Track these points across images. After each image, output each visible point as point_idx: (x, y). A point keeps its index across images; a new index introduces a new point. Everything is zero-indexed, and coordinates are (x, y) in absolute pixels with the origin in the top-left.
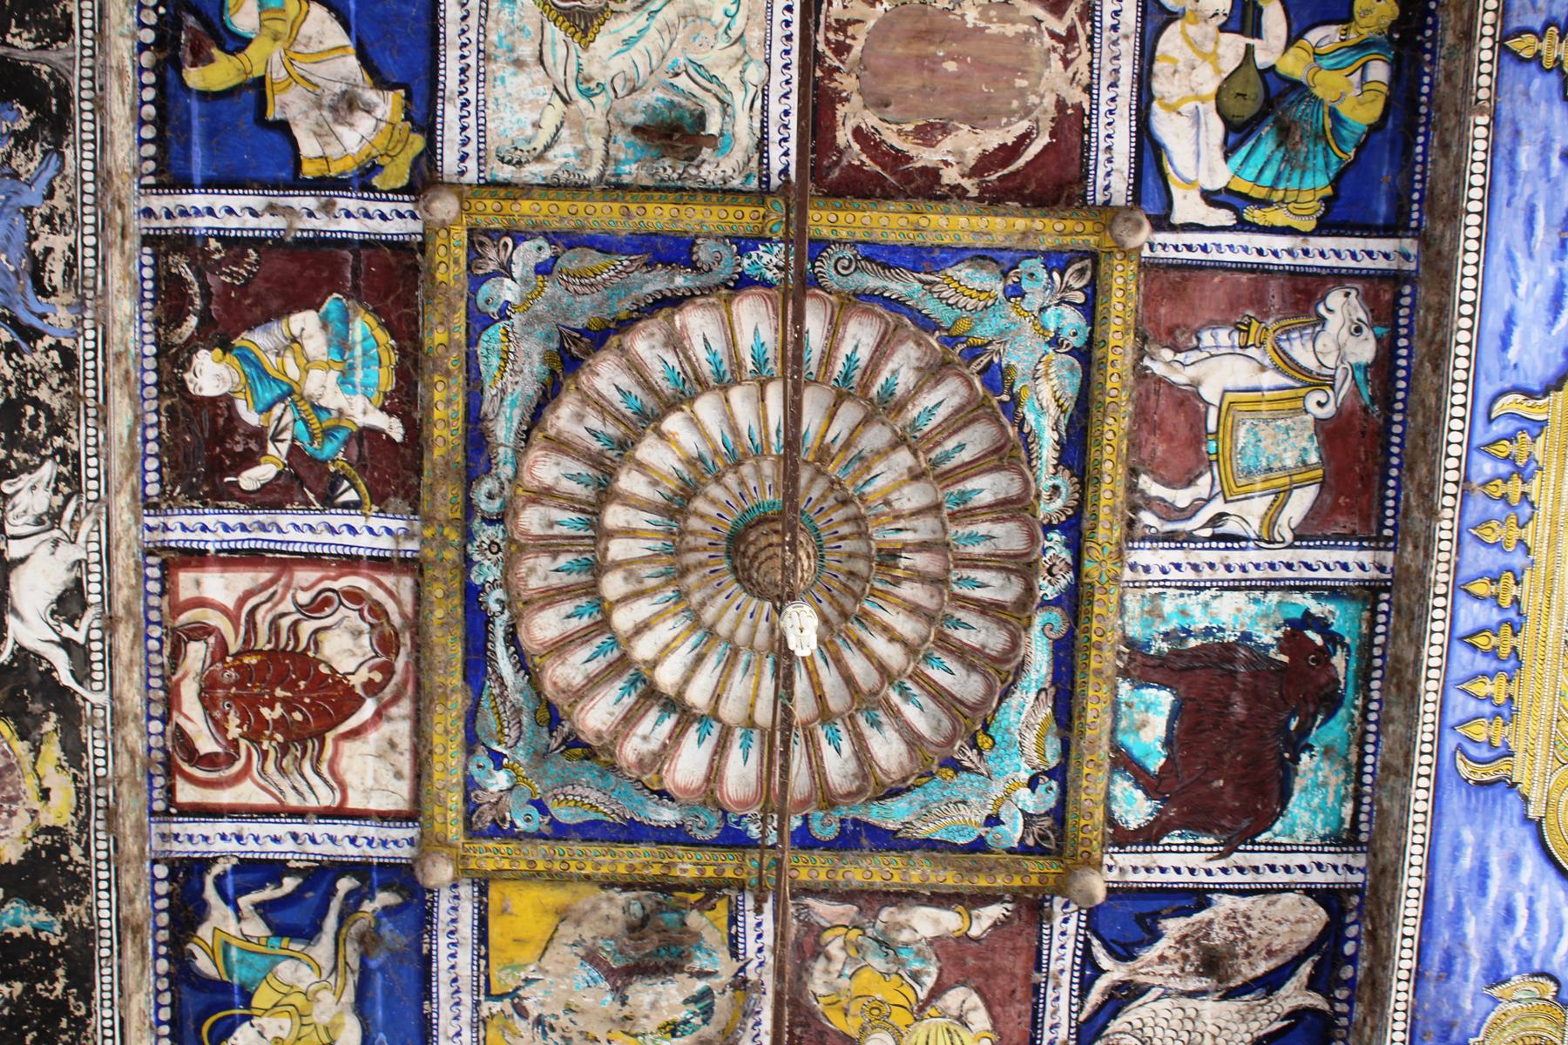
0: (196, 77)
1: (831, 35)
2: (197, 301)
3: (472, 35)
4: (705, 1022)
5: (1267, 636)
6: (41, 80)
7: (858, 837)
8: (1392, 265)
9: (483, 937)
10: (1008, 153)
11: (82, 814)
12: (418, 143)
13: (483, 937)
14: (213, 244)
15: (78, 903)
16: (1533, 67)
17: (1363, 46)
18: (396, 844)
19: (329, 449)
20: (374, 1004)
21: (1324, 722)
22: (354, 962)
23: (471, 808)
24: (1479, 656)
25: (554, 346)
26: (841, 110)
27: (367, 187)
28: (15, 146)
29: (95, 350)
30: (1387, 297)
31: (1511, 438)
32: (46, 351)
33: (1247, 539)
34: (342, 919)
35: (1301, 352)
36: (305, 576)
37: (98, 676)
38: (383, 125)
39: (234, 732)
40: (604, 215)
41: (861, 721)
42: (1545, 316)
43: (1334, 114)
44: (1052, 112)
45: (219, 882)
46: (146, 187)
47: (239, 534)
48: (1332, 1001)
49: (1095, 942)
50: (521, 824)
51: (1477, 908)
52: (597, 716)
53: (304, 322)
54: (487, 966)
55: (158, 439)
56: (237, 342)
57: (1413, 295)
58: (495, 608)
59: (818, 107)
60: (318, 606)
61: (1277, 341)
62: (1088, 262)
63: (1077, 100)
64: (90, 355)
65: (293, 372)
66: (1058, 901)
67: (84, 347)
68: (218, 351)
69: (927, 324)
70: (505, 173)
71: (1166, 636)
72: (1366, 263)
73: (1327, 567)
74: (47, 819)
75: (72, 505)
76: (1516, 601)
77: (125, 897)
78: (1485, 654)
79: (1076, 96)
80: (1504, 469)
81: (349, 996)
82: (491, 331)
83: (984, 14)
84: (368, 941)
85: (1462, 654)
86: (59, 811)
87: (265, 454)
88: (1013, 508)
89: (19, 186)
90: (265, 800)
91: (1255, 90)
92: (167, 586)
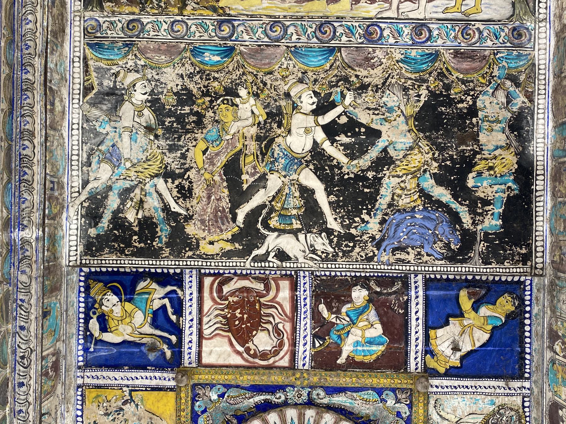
0: (463, 294)
2: (385, 291)
3: (479, 390)
9: (154, 389)
11: (204, 256)
12: (442, 370)
13: (154, 389)
14: (406, 298)
15: (170, 253)
18: (189, 358)
19: (334, 336)
20: (127, 348)
22: (144, 341)
23: (203, 386)
25: (372, 418)
27: (427, 352)
29: (373, 269)
32: (373, 251)
36: (288, 326)
37: (256, 264)
39: (231, 299)
45: (174, 292)
47: (303, 303)
53: (377, 330)
54: (142, 390)
55: (336, 275)
56: (371, 305)
58: (278, 396)
60: (278, 332)
64: (371, 267)
65: (361, 324)
70: (432, 402)
74: (202, 243)
75: (318, 258)
82: (377, 395)
84: (153, 348)
86: (205, 248)
87: (332, 314)
89: (431, 244)
90: (206, 309)
92: (284, 277)
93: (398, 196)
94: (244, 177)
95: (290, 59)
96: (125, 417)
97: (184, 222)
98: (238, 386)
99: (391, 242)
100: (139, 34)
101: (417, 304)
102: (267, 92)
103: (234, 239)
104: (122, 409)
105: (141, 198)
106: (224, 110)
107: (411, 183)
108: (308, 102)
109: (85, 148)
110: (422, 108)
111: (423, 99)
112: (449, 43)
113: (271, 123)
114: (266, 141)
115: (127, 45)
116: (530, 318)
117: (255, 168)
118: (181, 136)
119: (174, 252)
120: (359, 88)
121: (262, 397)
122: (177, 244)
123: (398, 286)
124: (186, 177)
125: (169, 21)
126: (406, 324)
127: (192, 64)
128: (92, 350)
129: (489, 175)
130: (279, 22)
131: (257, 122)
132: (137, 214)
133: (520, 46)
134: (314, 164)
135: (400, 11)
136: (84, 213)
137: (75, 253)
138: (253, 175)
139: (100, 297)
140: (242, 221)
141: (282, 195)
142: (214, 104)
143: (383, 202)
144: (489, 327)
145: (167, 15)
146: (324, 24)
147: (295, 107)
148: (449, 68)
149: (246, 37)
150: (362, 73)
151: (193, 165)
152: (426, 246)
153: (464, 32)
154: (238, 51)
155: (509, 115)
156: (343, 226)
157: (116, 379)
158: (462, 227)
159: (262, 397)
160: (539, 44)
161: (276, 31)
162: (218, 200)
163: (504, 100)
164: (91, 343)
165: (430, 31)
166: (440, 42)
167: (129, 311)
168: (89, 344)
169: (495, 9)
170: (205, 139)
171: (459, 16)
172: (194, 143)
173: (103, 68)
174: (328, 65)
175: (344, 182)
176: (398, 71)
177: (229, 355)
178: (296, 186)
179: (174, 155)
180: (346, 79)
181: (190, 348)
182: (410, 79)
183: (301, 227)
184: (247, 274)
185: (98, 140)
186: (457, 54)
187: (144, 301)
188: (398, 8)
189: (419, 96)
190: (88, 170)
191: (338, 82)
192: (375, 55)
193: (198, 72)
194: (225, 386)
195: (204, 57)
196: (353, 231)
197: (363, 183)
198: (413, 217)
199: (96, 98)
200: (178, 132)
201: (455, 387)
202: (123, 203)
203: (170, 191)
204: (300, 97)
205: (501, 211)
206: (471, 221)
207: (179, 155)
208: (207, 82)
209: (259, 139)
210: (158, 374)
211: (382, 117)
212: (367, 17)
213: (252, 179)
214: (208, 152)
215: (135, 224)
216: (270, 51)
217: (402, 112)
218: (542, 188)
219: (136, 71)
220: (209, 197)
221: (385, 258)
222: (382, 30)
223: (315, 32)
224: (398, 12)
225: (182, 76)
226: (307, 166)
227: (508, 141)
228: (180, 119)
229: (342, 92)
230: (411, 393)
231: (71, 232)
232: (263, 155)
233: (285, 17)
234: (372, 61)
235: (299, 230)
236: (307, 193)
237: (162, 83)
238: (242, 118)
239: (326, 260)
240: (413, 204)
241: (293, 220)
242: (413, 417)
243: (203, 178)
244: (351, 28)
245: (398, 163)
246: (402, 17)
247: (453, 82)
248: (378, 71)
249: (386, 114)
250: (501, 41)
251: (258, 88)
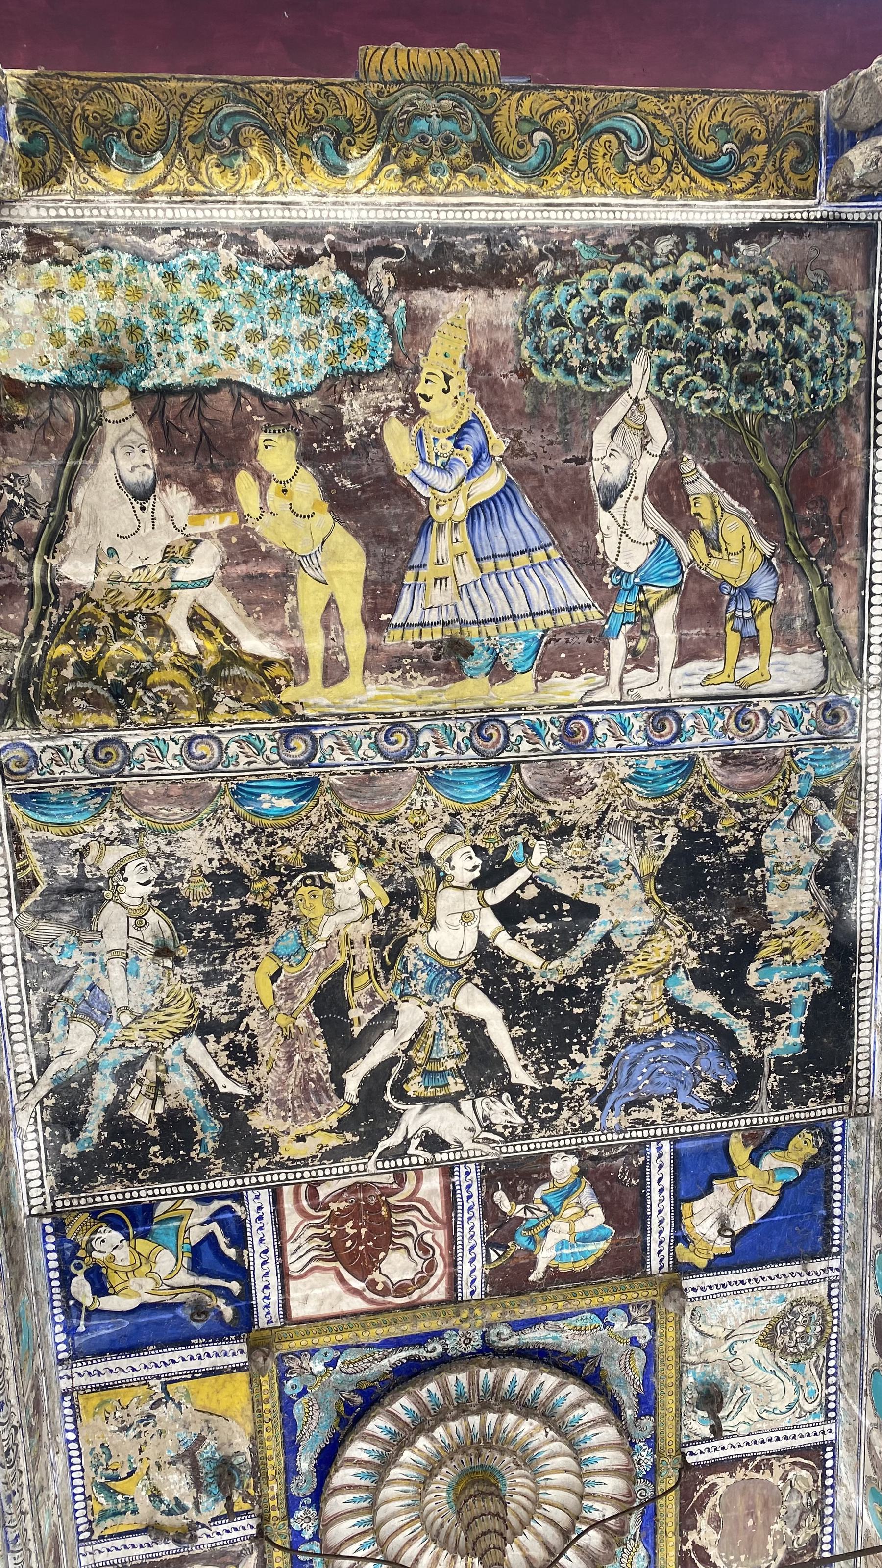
3: (762, 1283)
9: (206, 1374)
12: (702, 1263)
13: (206, 1374)
14: (641, 1160)
15: (224, 1168)
18: (266, 1311)
19: (522, 1239)
22: (180, 1298)
26: (725, 1475)
27: (677, 1240)
36: (441, 1236)
39: (334, 1206)
40: (667, 1372)
47: (465, 1195)
53: (598, 1215)
56: (584, 1179)
60: (424, 1247)
65: (568, 1213)
67: (595, 1136)
74: (283, 1142)
75: (497, 1138)
83: (778, 1532)
86: (289, 1149)
90: (289, 1230)
94: (354, 1014)
95: (428, 792)
96: (158, 1427)
97: (246, 1109)
100: (122, 767)
102: (386, 855)
103: (343, 1125)
104: (150, 1416)
105: (158, 1078)
106: (306, 896)
107: (653, 991)
108: (464, 866)
109: (33, 998)
110: (668, 860)
111: (669, 843)
112: (713, 740)
113: (398, 910)
114: (389, 944)
115: (98, 793)
116: (841, 1162)
117: (372, 994)
118: (227, 954)
119: (232, 1164)
120: (555, 834)
121: (404, 1354)
122: (235, 1150)
124: (242, 1027)
125: (181, 738)
127: (237, 818)
128: (82, 1329)
130: (402, 724)
131: (371, 912)
132: (153, 1107)
133: (836, 735)
134: (481, 976)
135: (626, 687)
136: (47, 1117)
137: (40, 1191)
138: (369, 1007)
139: (86, 1238)
141: (427, 1037)
142: (288, 887)
143: (606, 1028)
144: (778, 1186)
145: (176, 725)
146: (486, 721)
147: (441, 878)
148: (714, 785)
149: (340, 758)
150: (561, 805)
152: (681, 1093)
153: (740, 718)
154: (326, 785)
155: (818, 858)
156: (538, 1077)
157: (134, 1369)
158: (739, 1053)
159: (404, 1354)
160: (868, 730)
161: (397, 742)
163: (808, 833)
164: (79, 1318)
165: (679, 721)
166: (697, 739)
167: (145, 1254)
168: (74, 1321)
169: (794, 673)
170: (275, 954)
171: (730, 689)
172: (253, 964)
173: (52, 842)
174: (498, 797)
175: (536, 1002)
176: (624, 797)
177: (340, 1298)
178: (452, 1018)
179: (216, 990)
180: (532, 820)
181: (267, 1298)
182: (646, 809)
183: (464, 1088)
185: (59, 980)
186: (728, 759)
187: (172, 1233)
188: (621, 683)
189: (662, 838)
190: (45, 1039)
191: (517, 825)
192: (582, 772)
193: (251, 832)
194: (335, 1348)
195: (261, 802)
196: (557, 1084)
198: (658, 1047)
199: (46, 902)
200: (219, 947)
201: (723, 1286)
202: (124, 1089)
203: (214, 1056)
204: (449, 860)
205: (803, 1019)
206: (753, 1043)
207: (225, 989)
208: (270, 849)
209: (376, 941)
210: (211, 1349)
211: (599, 881)
212: (566, 702)
213: (370, 1016)
214: (282, 977)
215: (152, 1126)
216: (388, 780)
217: (633, 869)
218: (869, 974)
219: (122, 842)
220: (290, 1059)
221: (613, 1122)
222: (593, 725)
223: (470, 739)
224: (621, 689)
225: (219, 842)
226: (470, 980)
227: (814, 904)
228: (223, 923)
229: (525, 844)
231: (27, 1156)
232: (387, 969)
233: (412, 714)
234: (578, 783)
235: (462, 1094)
236: (472, 1028)
237: (179, 860)
238: (343, 908)
239: (513, 1137)
240: (657, 1026)
242: (657, 1343)
243: (275, 1026)
244: (537, 725)
245: (629, 957)
246: (630, 699)
247: (720, 808)
248: (589, 800)
249: (606, 875)
250: (803, 728)
251: (369, 851)
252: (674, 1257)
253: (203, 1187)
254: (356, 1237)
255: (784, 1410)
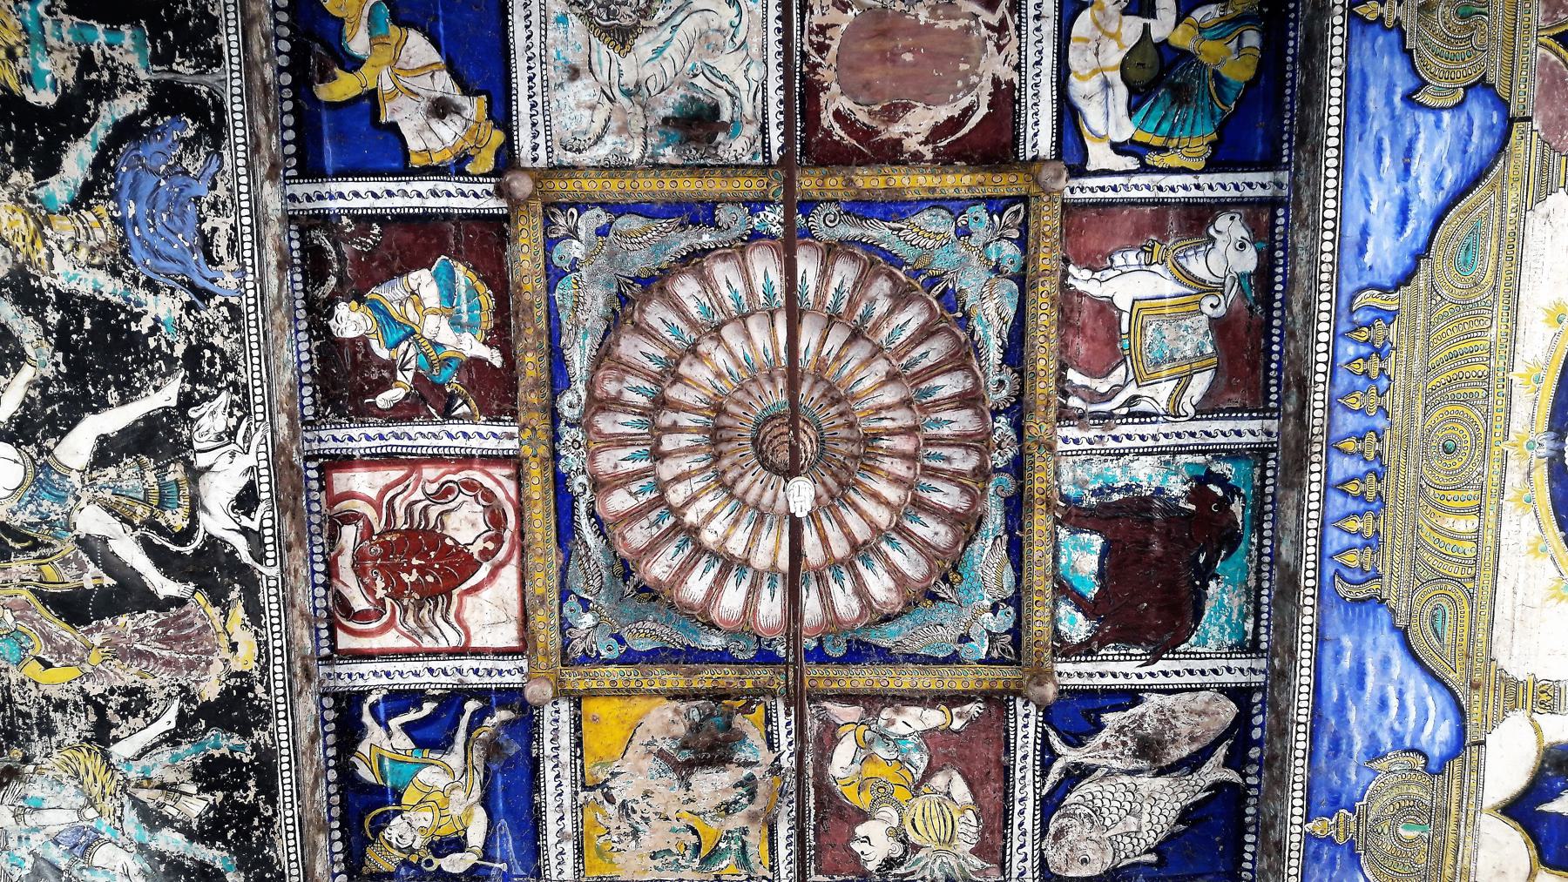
1: (813, 38)
4: (750, 801)
5: (1177, 487)
6: (201, 97)
7: (858, 653)
8: (1268, 193)
10: (954, 124)
12: (498, 137)
14: (345, 220)
15: (264, 729)
16: (1377, 27)
17: (1238, 21)
18: (509, 674)
21: (1228, 555)
24: (1349, 500)
26: (823, 98)
28: (185, 149)
29: (255, 305)
30: (1265, 218)
31: (1370, 325)
32: (217, 307)
33: (1157, 415)
34: (469, 732)
35: (1197, 266)
36: (429, 472)
37: (270, 555)
38: (471, 124)
39: (380, 593)
40: (648, 186)
41: (859, 564)
42: (1392, 228)
43: (1216, 75)
44: (989, 88)
45: (373, 709)
46: (290, 178)
47: (378, 442)
48: (1244, 776)
49: (1052, 733)
50: (605, 654)
51: (1357, 700)
52: (659, 569)
53: (422, 280)
56: (368, 295)
57: (1286, 216)
58: (579, 490)
59: (803, 95)
60: (443, 493)
61: (1176, 258)
62: (1021, 206)
63: (1008, 78)
65: (412, 315)
66: (1019, 703)
67: (247, 303)
68: (354, 303)
69: (893, 260)
70: (569, 158)
71: (1094, 493)
72: (1248, 193)
73: (1224, 434)
74: (237, 666)
75: (244, 425)
76: (1379, 455)
77: (294, 729)
78: (1355, 498)
79: (1006, 73)
80: (1364, 350)
81: (477, 793)
84: (493, 748)
85: (1337, 500)
86: (246, 658)
88: (967, 400)
90: (406, 643)
91: (1151, 58)
93: (94, 256)
94: (89, 584)
98: (564, 571)
99: (194, 267)
101: (356, 194)
104: (623, 805)
117: (65, 562)
118: (19, 712)
122: (243, 716)
123: (321, 238)
126: (405, 220)
128: (504, 867)
129: (25, 56)
134: (45, 438)
138: (82, 567)
139: (396, 853)
140: (182, 587)
141: (118, 503)
143: (112, 289)
144: (395, 31)
151: (76, 685)
152: (196, 193)
156: (170, 373)
158: (145, 115)
162: (143, 636)
172: (30, 685)
175: (77, 371)
178: (95, 474)
179: (59, 724)
184: (325, 561)
187: (398, 767)
196: (179, 350)
197: (74, 332)
202: (168, 822)
205: (100, 28)
213: (91, 566)
214: (46, 657)
221: (230, 281)
226: (50, 452)
230: (552, 207)
232: (36, 545)
235: (189, 465)
236: (106, 453)
240: (107, 223)
241: (168, 479)
252: (485, 175)
253: (285, 752)
254: (422, 571)
255: (735, 10)
